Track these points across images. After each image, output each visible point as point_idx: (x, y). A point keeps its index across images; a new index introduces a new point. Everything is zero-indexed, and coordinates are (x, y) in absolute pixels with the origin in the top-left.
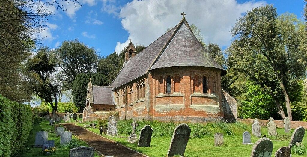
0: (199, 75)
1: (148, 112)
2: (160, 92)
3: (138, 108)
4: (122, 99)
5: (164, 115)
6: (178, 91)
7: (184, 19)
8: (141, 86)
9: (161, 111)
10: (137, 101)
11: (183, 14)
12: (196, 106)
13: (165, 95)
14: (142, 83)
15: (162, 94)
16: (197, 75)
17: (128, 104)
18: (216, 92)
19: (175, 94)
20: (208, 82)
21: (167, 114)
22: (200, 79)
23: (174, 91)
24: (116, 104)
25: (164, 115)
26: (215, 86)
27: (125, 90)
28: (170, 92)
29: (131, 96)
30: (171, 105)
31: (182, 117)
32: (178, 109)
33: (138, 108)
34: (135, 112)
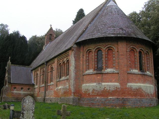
0: (134, 50)
1: (74, 92)
2: (89, 69)
3: (60, 87)
4: (40, 78)
5: (94, 96)
6: (112, 68)
7: (52, 27)
8: (64, 62)
9: (91, 91)
10: (58, 80)
11: (51, 25)
12: (134, 85)
13: (95, 72)
14: (61, 61)
15: (91, 71)
16: (132, 49)
17: (47, 83)
18: (150, 70)
19: (109, 70)
20: (143, 59)
21: (98, 95)
22: (136, 54)
23: (107, 67)
24: (35, 84)
25: (94, 96)
26: (149, 64)
27: (45, 69)
28: (101, 69)
29: (51, 74)
30: (103, 84)
31: (117, 98)
32: (112, 89)
33: (60, 87)
34: (56, 93)
